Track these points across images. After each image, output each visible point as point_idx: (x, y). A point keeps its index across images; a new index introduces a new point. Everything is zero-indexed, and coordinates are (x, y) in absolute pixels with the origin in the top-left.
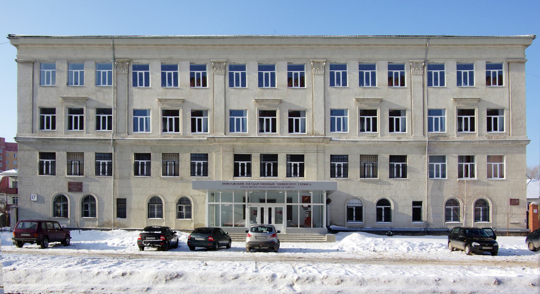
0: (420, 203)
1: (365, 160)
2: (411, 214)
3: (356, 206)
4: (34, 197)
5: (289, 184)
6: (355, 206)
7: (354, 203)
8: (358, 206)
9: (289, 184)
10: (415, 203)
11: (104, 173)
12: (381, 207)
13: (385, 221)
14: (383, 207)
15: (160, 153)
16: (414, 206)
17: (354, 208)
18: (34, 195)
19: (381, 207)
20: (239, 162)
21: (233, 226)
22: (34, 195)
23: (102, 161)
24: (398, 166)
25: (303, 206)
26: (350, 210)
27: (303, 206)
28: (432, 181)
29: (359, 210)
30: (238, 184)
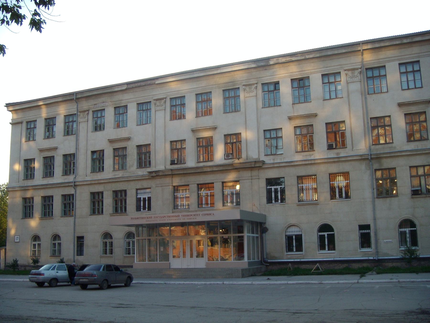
0: (368, 227)
1: (145, 195)
2: (100, 247)
3: (296, 234)
4: (17, 238)
5: (193, 215)
6: (294, 234)
7: (293, 231)
8: (297, 234)
9: (193, 215)
10: (361, 227)
11: (276, 200)
12: (322, 233)
13: (296, 251)
14: (326, 234)
15: (39, 196)
16: (361, 230)
17: (294, 237)
18: (18, 236)
19: (322, 233)
20: (272, 187)
21: (219, 259)
22: (18, 236)
23: (274, 187)
24: (276, 191)
25: (223, 237)
26: (289, 239)
27: (223, 237)
28: (336, 202)
29: (299, 238)
30: (147, 218)
